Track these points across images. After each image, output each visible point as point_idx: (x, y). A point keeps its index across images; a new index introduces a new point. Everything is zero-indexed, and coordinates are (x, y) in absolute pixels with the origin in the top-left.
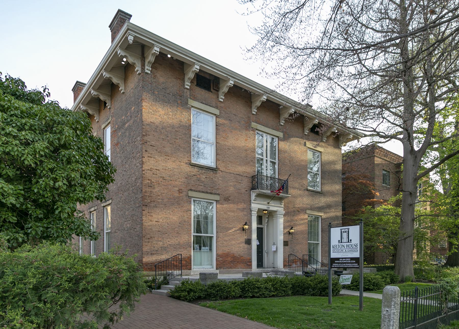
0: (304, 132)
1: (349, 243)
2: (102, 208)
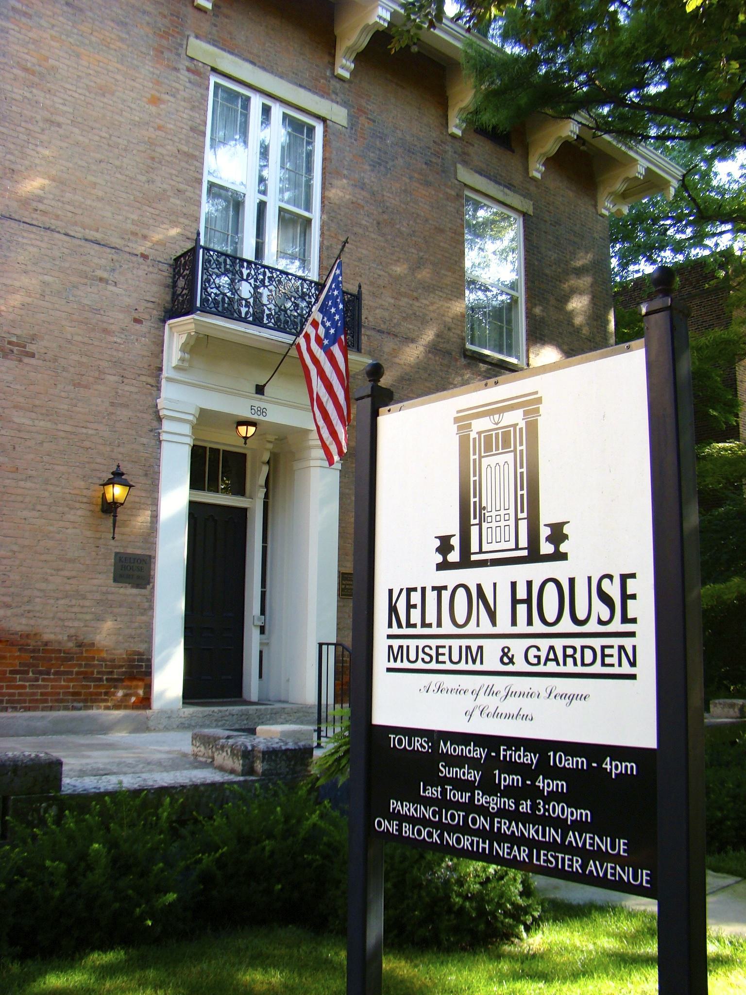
0: (446, 125)
1: (537, 572)
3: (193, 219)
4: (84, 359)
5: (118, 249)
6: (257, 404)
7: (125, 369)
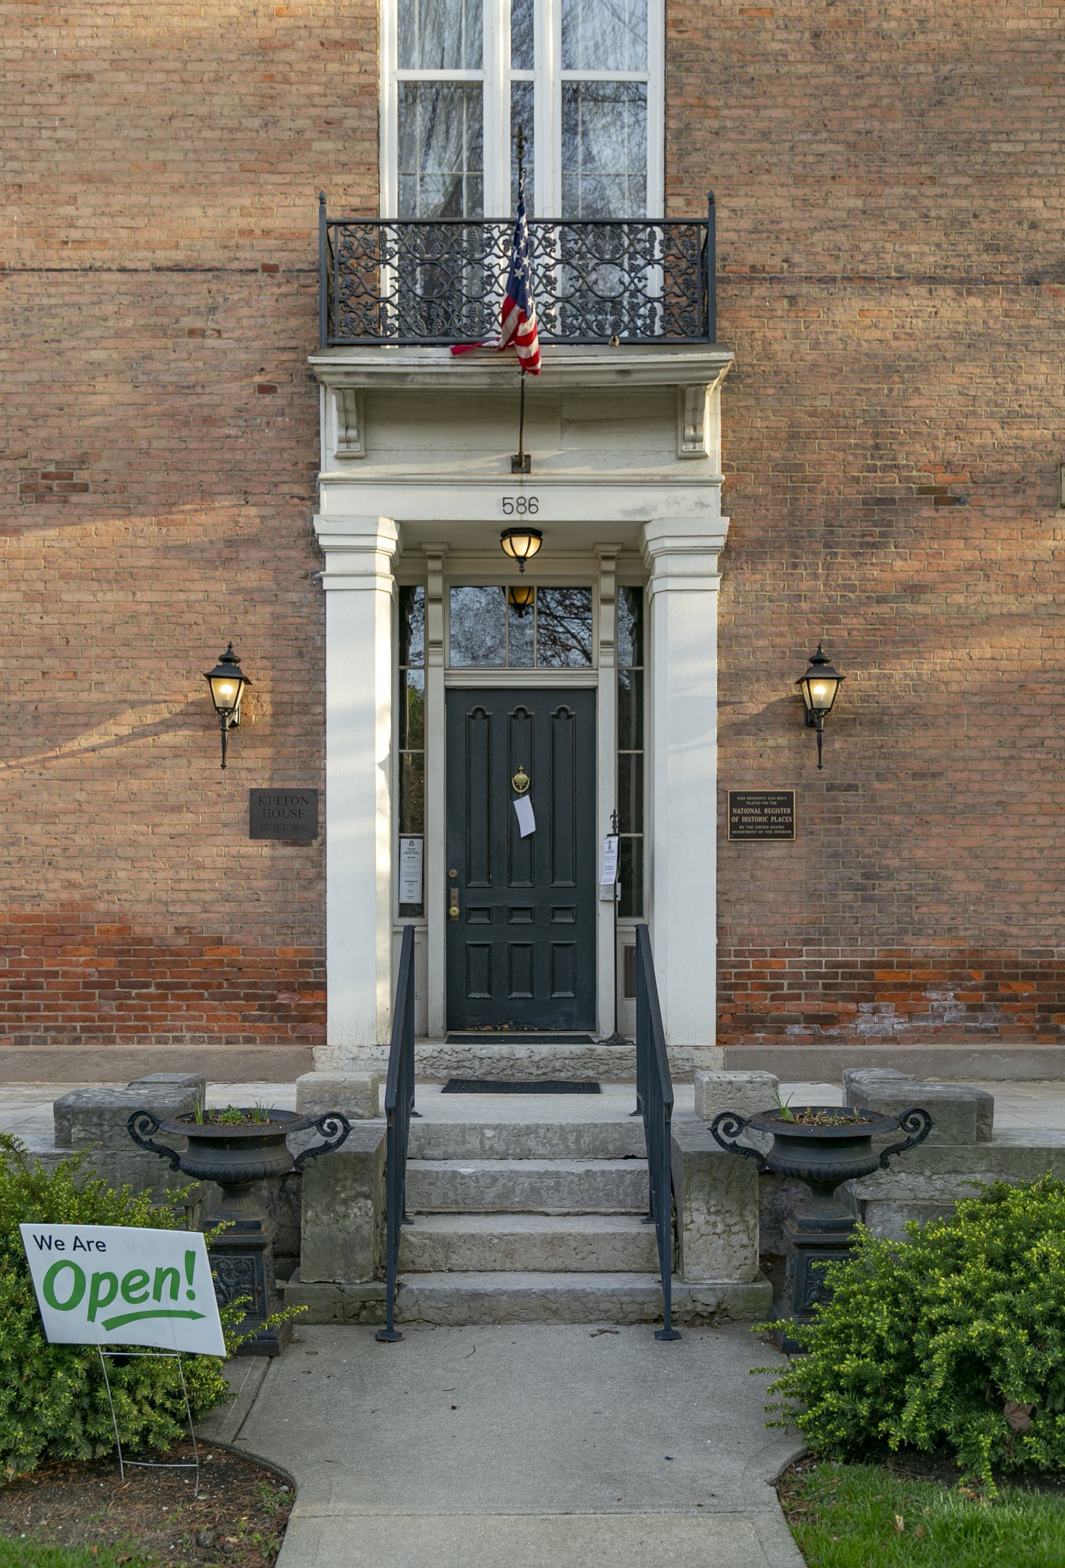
3: (363, 169)
4: (174, 477)
5: (218, 270)
6: (515, 493)
7: (247, 480)
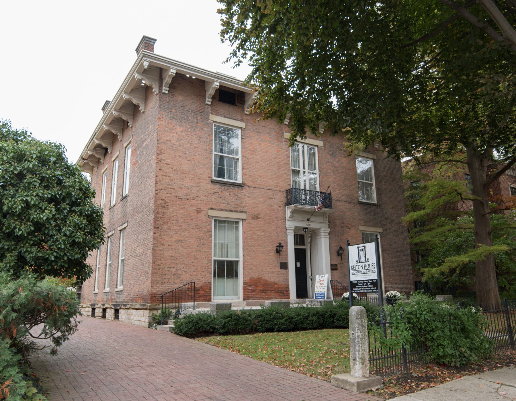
2: (119, 232)
6: (308, 223)
